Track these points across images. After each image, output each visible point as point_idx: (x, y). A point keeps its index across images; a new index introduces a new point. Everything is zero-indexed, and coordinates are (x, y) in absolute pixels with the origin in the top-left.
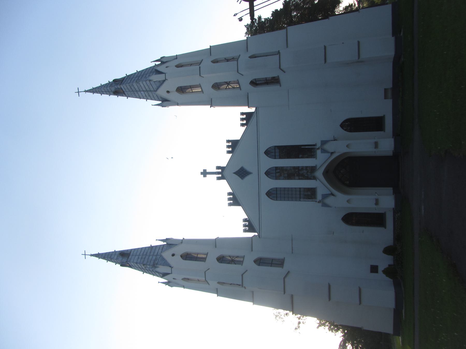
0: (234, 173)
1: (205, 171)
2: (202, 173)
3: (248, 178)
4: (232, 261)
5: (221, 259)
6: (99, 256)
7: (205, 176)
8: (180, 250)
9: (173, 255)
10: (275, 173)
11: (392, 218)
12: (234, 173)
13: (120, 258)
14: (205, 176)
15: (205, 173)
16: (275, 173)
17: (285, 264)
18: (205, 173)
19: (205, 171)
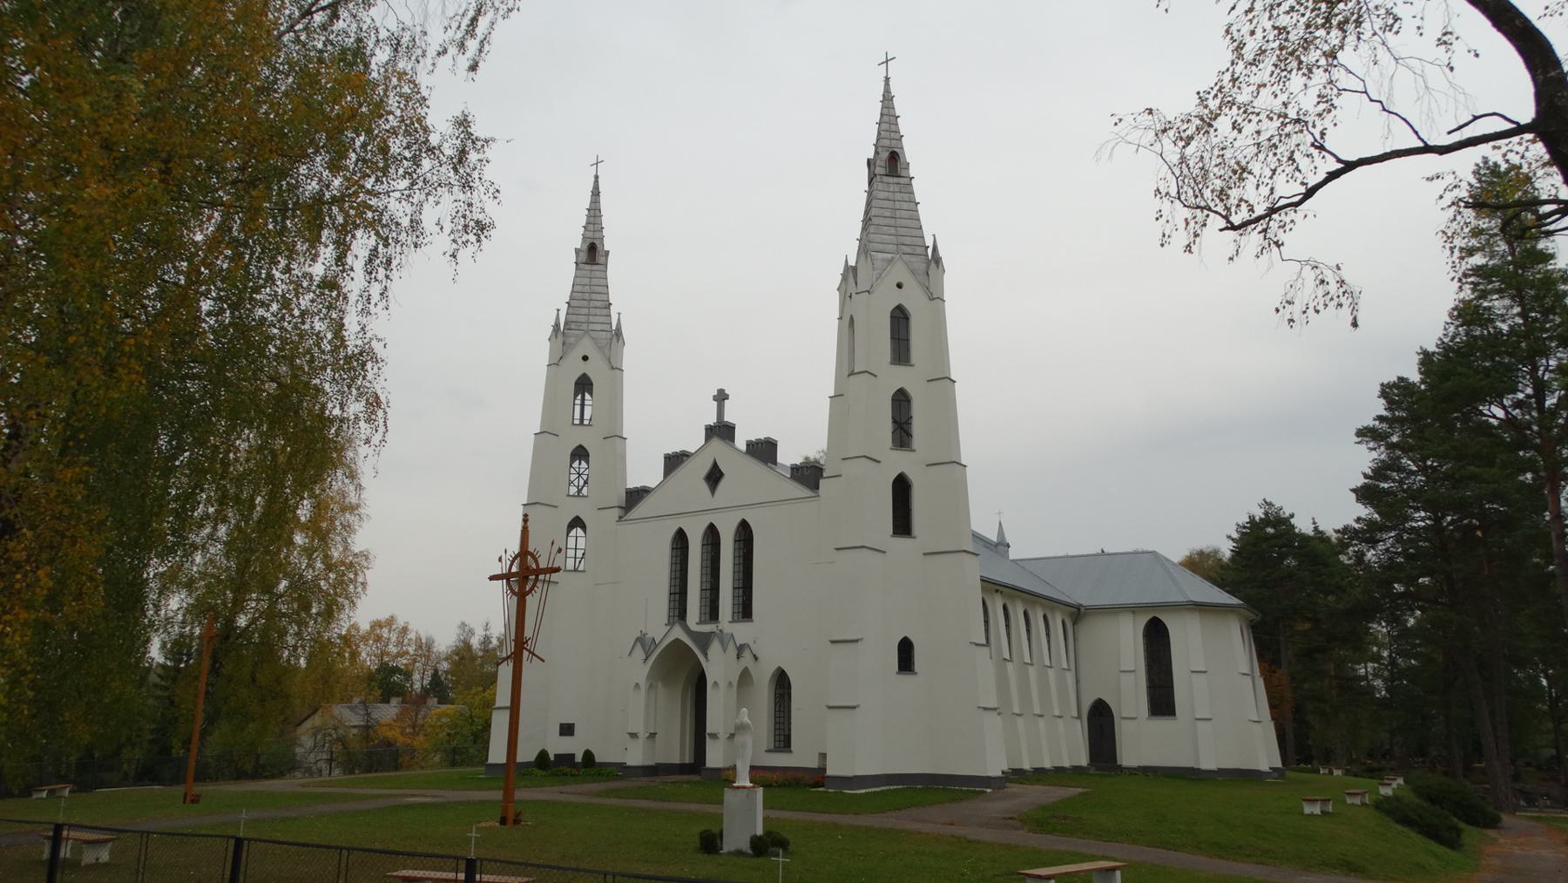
0: (715, 465)
1: (727, 397)
2: (721, 391)
3: (705, 487)
4: (902, 433)
5: (901, 400)
6: (887, 99)
7: (715, 398)
8: (913, 301)
9: (899, 286)
10: (712, 534)
11: (270, 782)
12: (715, 465)
13: (885, 155)
14: (715, 398)
15: (721, 397)
16: (712, 534)
17: (902, 542)
18: (721, 397)
19: (727, 397)
